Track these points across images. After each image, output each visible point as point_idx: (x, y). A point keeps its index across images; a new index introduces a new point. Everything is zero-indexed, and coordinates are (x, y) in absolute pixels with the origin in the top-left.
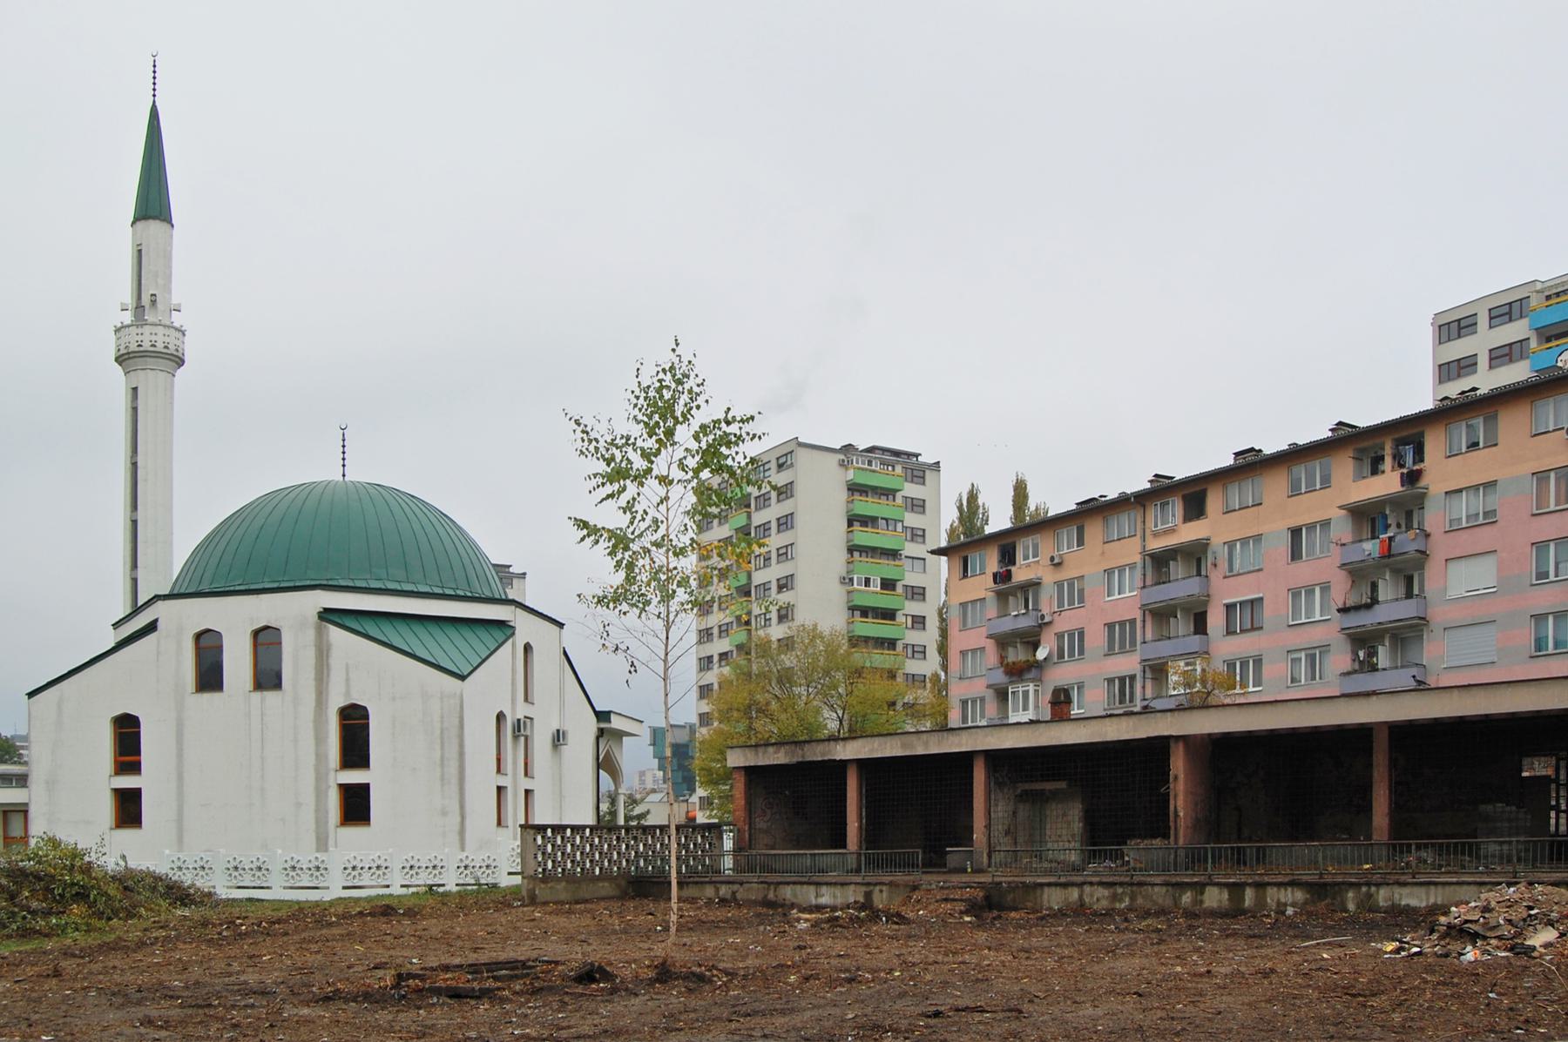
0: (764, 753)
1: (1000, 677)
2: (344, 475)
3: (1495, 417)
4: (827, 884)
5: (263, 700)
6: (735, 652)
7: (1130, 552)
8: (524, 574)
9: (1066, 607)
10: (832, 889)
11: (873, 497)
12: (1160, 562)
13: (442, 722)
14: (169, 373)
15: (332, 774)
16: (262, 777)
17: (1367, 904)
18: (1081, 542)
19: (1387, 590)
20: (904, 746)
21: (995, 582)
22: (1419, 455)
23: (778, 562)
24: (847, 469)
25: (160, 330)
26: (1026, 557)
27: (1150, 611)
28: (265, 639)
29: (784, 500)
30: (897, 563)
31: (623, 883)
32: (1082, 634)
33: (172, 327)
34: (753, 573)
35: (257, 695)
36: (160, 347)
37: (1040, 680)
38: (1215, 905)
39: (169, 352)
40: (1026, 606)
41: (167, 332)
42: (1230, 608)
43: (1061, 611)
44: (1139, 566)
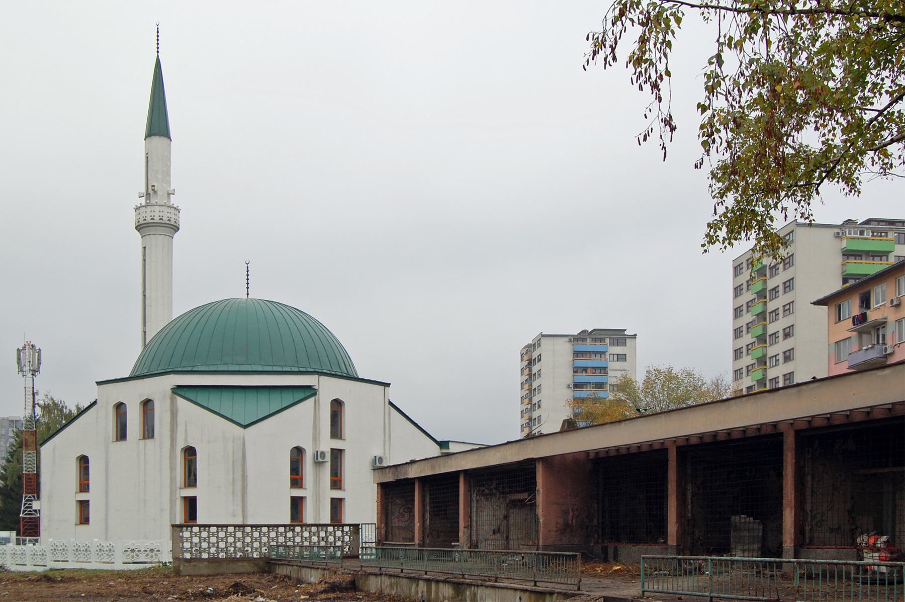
2: (248, 294)
5: (145, 445)
6: (756, 386)
8: (635, 335)
11: (866, 259)
13: (233, 456)
14: (170, 236)
15: (178, 490)
20: (433, 468)
23: (784, 316)
25: (157, 208)
29: (788, 268)
31: (261, 563)
33: (173, 207)
34: (768, 326)
35: (142, 442)
36: (157, 219)
39: (163, 222)
41: (169, 210)
43: (899, 344)
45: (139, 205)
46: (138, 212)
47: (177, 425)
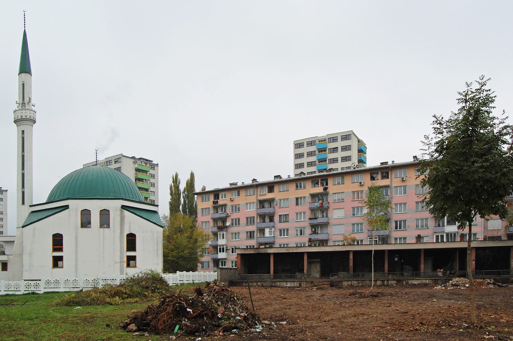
0: (247, 250)
1: (215, 229)
3: (344, 177)
4: (289, 282)
5: (104, 231)
7: (253, 199)
8: (7, 190)
9: (234, 212)
10: (290, 283)
12: (262, 203)
13: (157, 239)
16: (103, 253)
17: (407, 283)
18: (239, 195)
19: (319, 215)
21: (214, 204)
22: (327, 184)
24: (135, 164)
25: (28, 111)
26: (222, 198)
27: (259, 215)
28: (105, 214)
30: (148, 193)
32: (239, 220)
33: (32, 110)
35: (102, 229)
36: (28, 117)
37: (227, 231)
38: (379, 284)
40: (222, 211)
42: (280, 216)
44: (256, 203)
45: (15, 110)
46: (15, 113)
47: (124, 223)
